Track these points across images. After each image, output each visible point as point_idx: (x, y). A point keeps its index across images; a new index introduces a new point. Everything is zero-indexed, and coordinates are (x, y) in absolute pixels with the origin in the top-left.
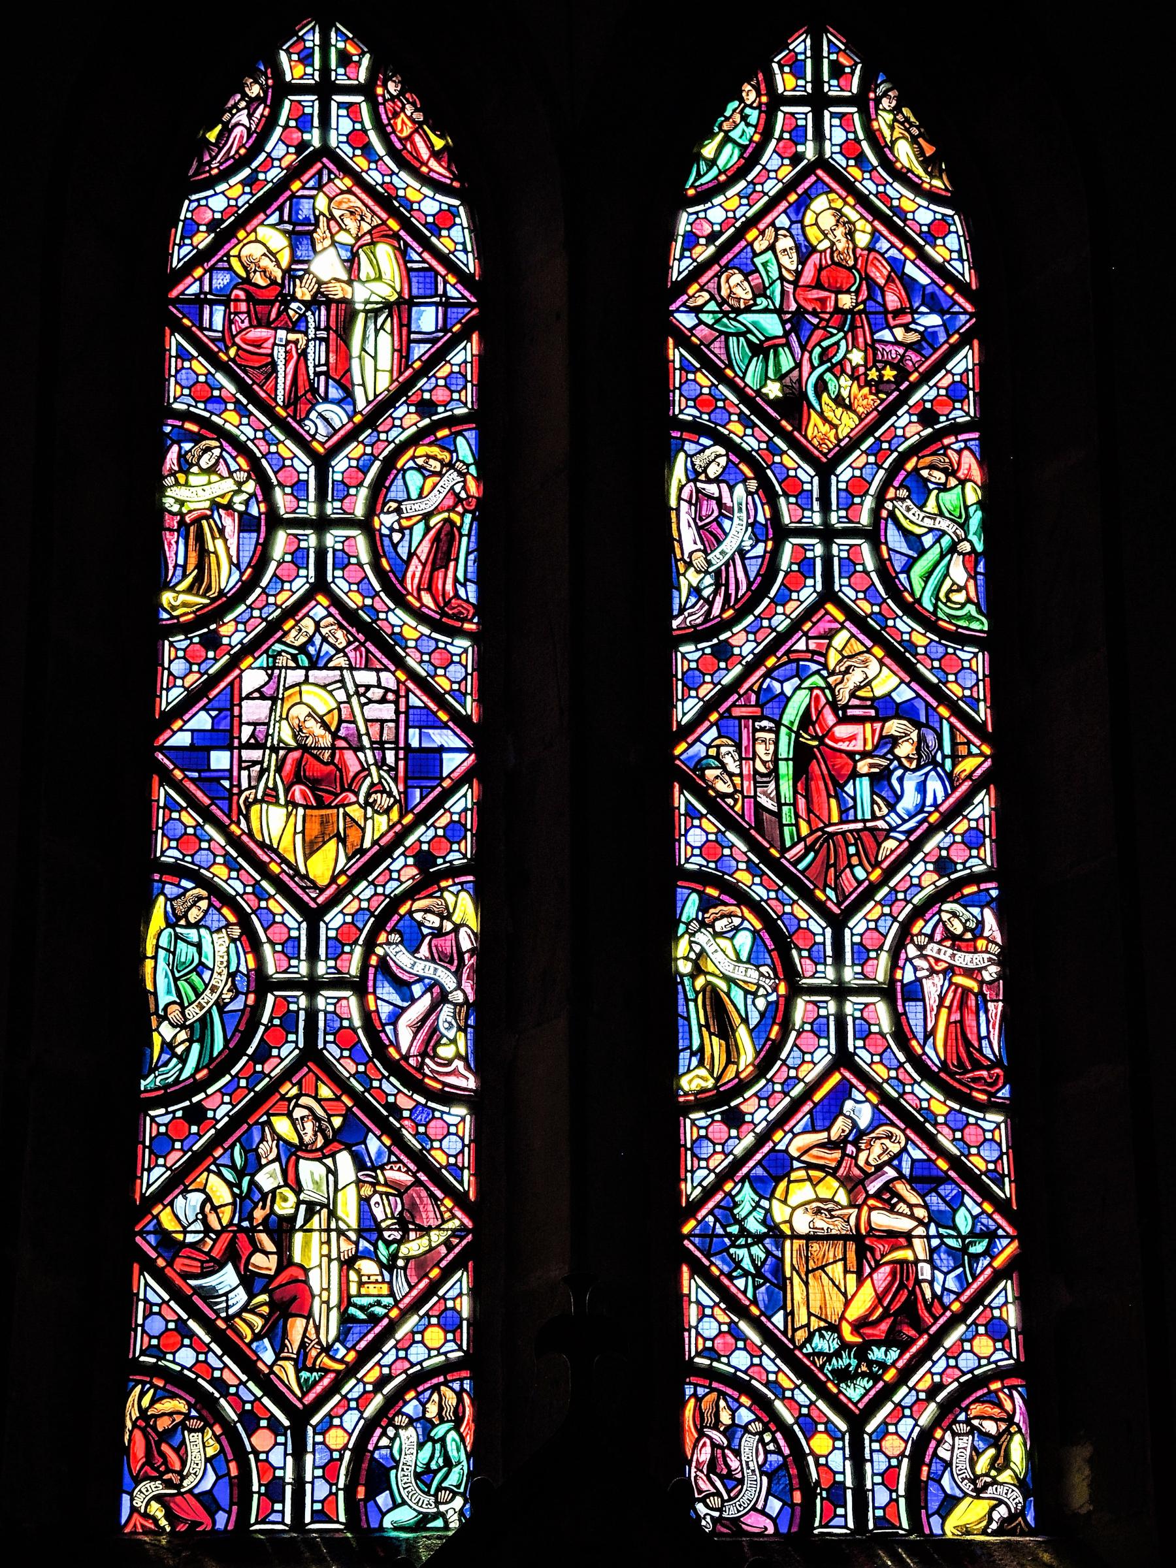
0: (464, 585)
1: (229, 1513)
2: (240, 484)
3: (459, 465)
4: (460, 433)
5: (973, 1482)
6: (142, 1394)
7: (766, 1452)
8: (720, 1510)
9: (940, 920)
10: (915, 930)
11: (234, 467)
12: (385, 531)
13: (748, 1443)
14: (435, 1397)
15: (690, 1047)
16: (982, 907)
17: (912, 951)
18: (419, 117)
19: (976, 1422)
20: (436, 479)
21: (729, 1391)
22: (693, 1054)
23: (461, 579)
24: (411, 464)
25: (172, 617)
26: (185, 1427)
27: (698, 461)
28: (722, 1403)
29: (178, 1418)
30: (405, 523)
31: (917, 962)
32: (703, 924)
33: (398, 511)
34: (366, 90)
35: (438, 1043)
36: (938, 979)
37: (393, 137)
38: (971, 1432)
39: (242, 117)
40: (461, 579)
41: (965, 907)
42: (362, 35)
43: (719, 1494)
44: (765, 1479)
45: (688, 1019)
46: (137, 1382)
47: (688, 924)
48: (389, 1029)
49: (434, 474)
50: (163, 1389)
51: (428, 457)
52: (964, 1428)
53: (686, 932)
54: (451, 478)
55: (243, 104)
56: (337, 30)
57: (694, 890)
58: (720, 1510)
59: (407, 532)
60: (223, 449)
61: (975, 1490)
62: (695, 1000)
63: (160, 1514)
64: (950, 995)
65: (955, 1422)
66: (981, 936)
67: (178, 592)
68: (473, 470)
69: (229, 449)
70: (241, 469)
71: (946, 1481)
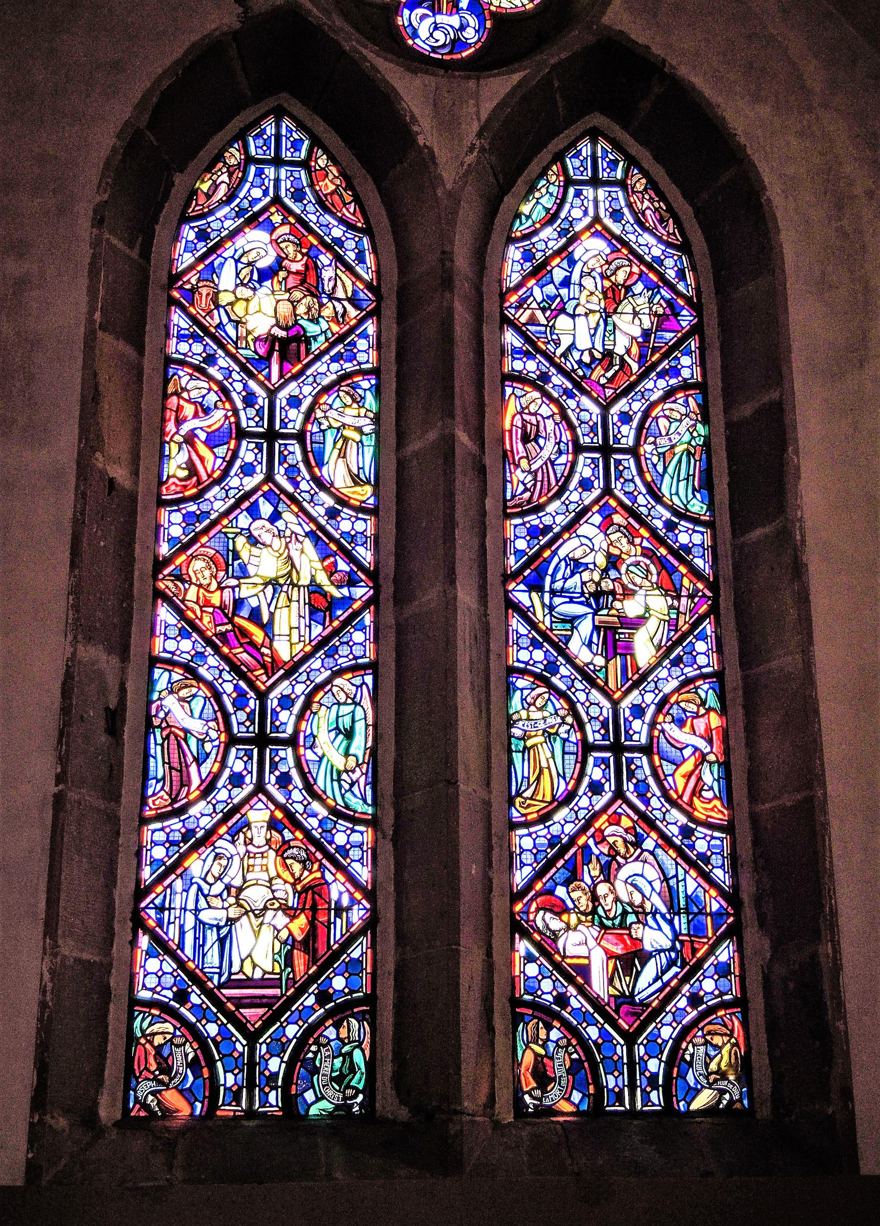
4: (691, 395)
5: (707, 1078)
6: (143, 1020)
12: (648, 456)
19: (709, 1038)
20: (678, 424)
22: (158, 781)
24: (661, 414)
26: (172, 1043)
27: (523, 400)
29: (169, 1037)
33: (654, 443)
34: (305, 164)
35: (702, 790)
39: (225, 178)
46: (141, 1012)
47: (160, 692)
48: (670, 779)
49: (676, 420)
50: (159, 1016)
52: (701, 1041)
55: (224, 170)
57: (166, 670)
58: (540, 1100)
61: (708, 1083)
65: (695, 1036)
71: (690, 1078)
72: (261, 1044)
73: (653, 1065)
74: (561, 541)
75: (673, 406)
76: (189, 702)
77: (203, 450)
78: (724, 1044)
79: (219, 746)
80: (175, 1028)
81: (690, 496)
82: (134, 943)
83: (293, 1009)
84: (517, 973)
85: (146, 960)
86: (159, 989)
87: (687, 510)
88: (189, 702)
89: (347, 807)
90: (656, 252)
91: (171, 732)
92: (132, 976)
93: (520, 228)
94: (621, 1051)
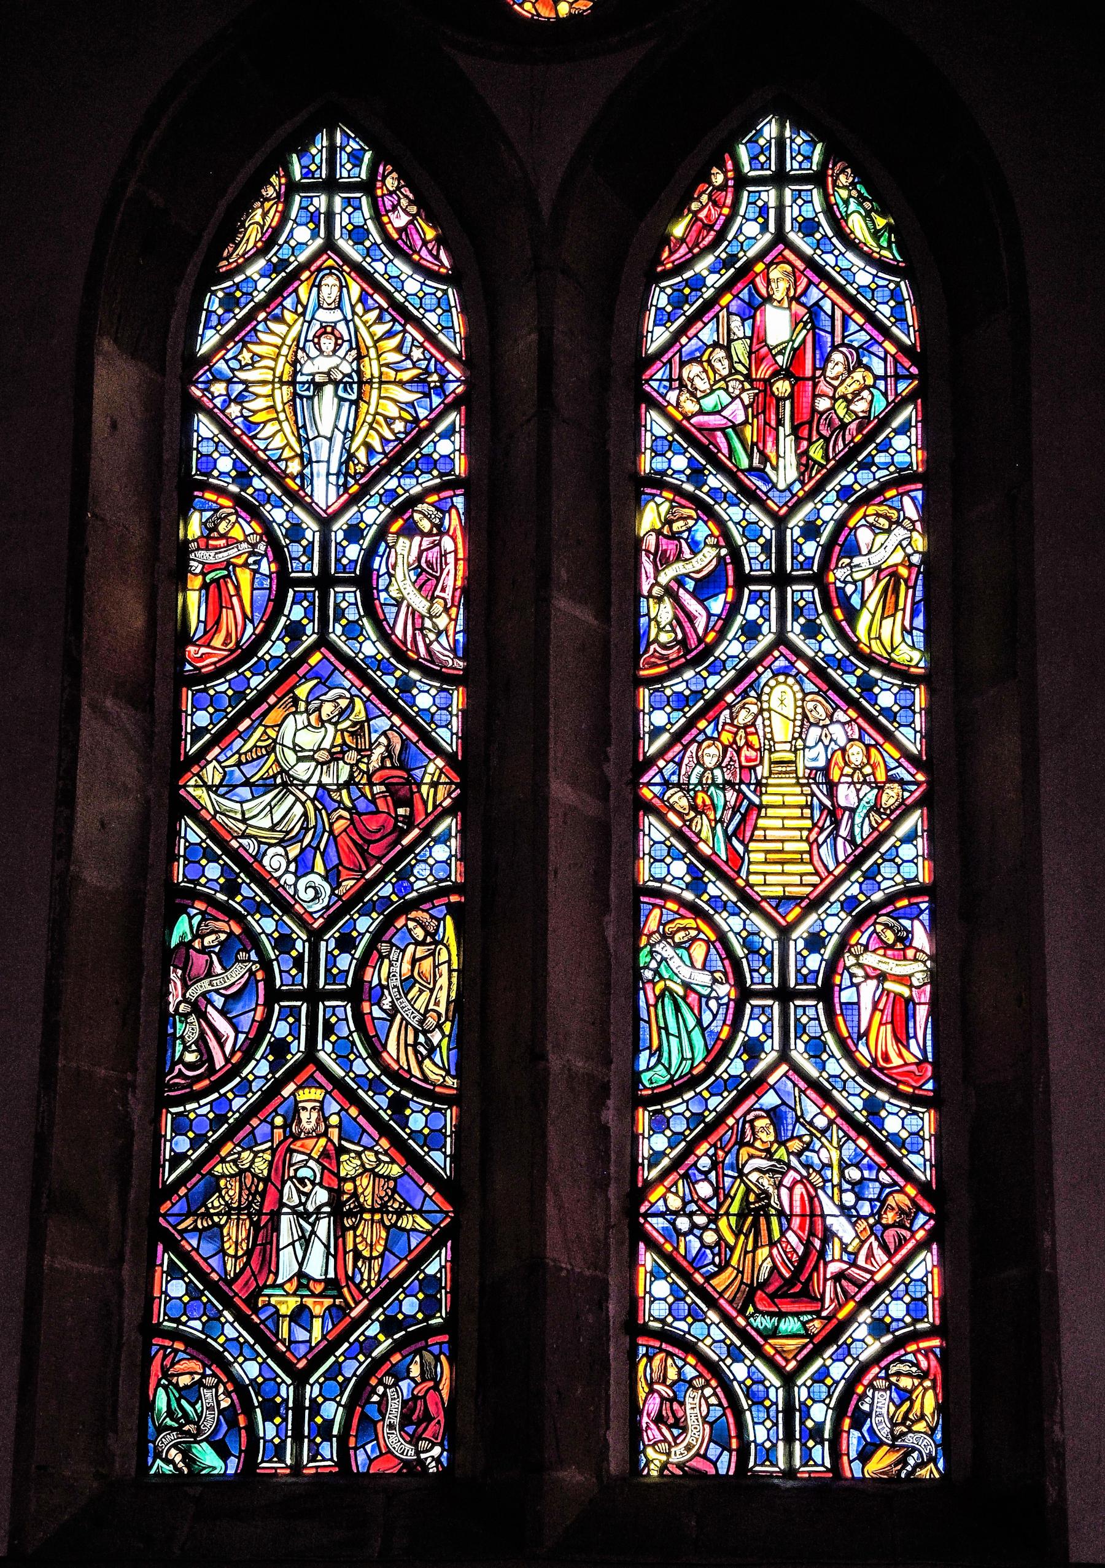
0: (910, 633)
1: (239, 1458)
2: (254, 546)
3: (906, 523)
4: (907, 493)
7: (709, 1405)
8: (668, 1454)
9: (875, 931)
10: (853, 941)
11: (248, 530)
13: (692, 1399)
14: (417, 1358)
15: (650, 1048)
16: (912, 920)
17: (850, 960)
18: (413, 209)
19: (893, 1379)
20: (885, 536)
21: (676, 1351)
23: (908, 627)
24: (863, 522)
25: (196, 668)
28: (670, 1361)
29: (197, 1377)
30: (857, 576)
31: (854, 970)
32: (664, 937)
34: (368, 187)
36: (873, 983)
37: (389, 226)
38: (889, 1388)
40: (908, 627)
41: (896, 919)
42: (362, 134)
43: (665, 1440)
44: (707, 1427)
45: (649, 1022)
47: (649, 936)
51: (878, 515)
53: (648, 943)
54: (899, 533)
56: (342, 131)
59: (859, 584)
60: (238, 516)
62: (655, 1006)
63: (178, 1458)
64: (884, 999)
66: (910, 946)
67: (200, 646)
68: (918, 525)
69: (243, 514)
70: (255, 533)
72: (312, 1386)
73: (329, 1410)
74: (265, 706)
75: (883, 509)
76: (688, 949)
77: (693, 605)
78: (915, 1388)
79: (727, 1004)
80: (204, 1366)
81: (898, 639)
82: (633, 1262)
83: (352, 1340)
84: (641, 1294)
85: (651, 1283)
86: (184, 1319)
87: (891, 660)
88: (688, 949)
89: (425, 1079)
90: (863, 279)
91: (666, 988)
92: (150, 1300)
93: (668, 258)
94: (286, 1392)
